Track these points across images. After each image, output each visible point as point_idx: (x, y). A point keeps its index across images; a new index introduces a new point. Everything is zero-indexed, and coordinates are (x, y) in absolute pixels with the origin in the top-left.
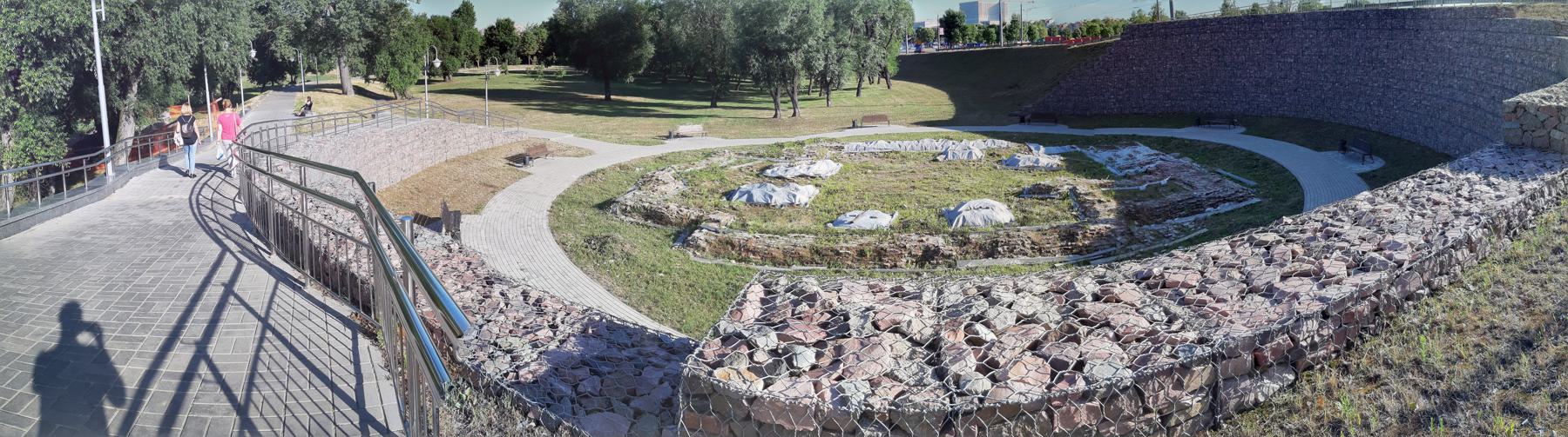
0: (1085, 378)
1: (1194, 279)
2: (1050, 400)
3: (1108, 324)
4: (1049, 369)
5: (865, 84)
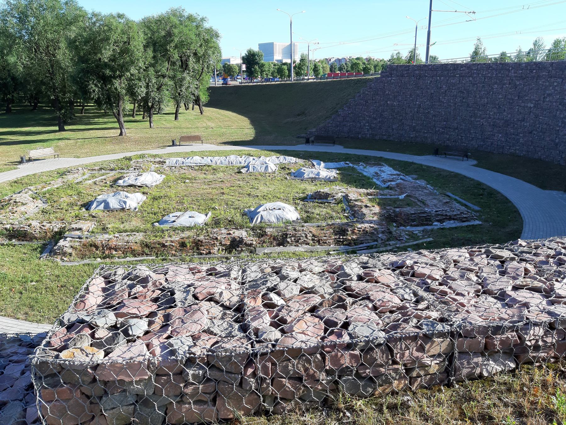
0: (350, 335)
1: (438, 274)
2: (323, 347)
3: (368, 298)
4: (323, 326)
5: (182, 109)
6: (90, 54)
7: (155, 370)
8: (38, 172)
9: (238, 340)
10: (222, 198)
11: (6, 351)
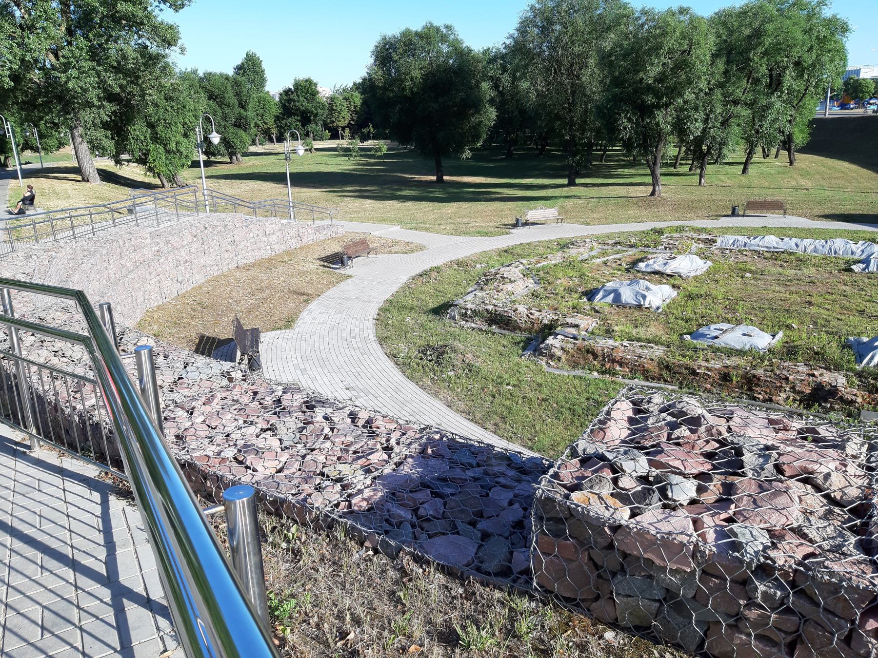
5: (757, 157)
6: (628, 73)
7: (703, 563)
8: (533, 240)
9: (854, 563)
10: (807, 310)
11: (493, 468)
